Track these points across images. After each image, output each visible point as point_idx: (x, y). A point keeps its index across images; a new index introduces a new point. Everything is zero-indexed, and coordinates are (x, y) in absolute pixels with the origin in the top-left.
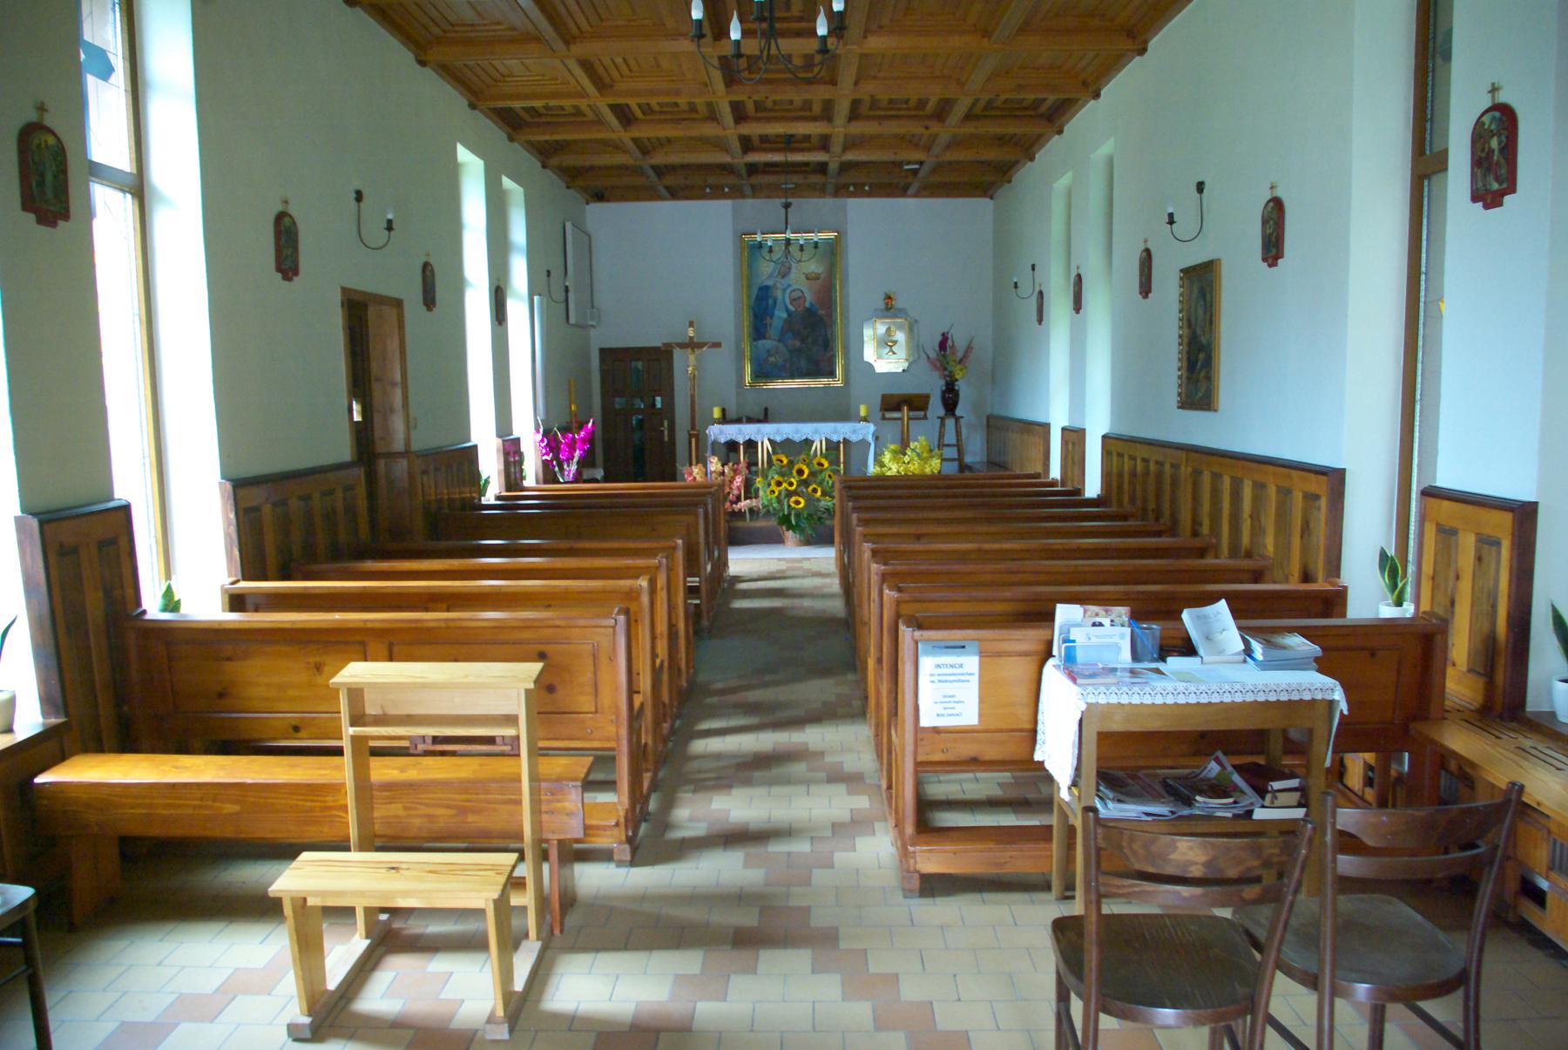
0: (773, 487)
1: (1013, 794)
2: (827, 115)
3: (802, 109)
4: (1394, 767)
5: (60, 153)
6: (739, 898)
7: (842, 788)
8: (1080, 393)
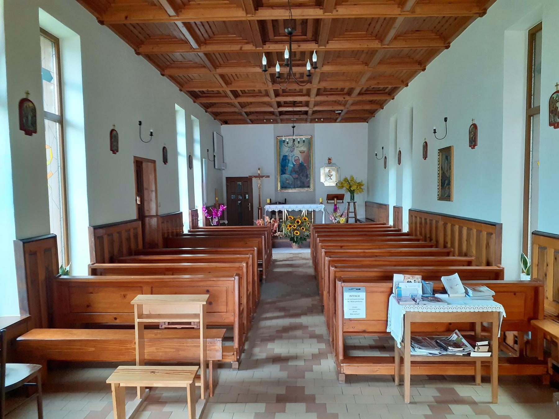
0: (288, 227)
1: (379, 344)
2: (308, 94)
3: (299, 92)
4: (525, 337)
5: (34, 110)
6: (278, 382)
7: (315, 340)
8: (402, 194)
